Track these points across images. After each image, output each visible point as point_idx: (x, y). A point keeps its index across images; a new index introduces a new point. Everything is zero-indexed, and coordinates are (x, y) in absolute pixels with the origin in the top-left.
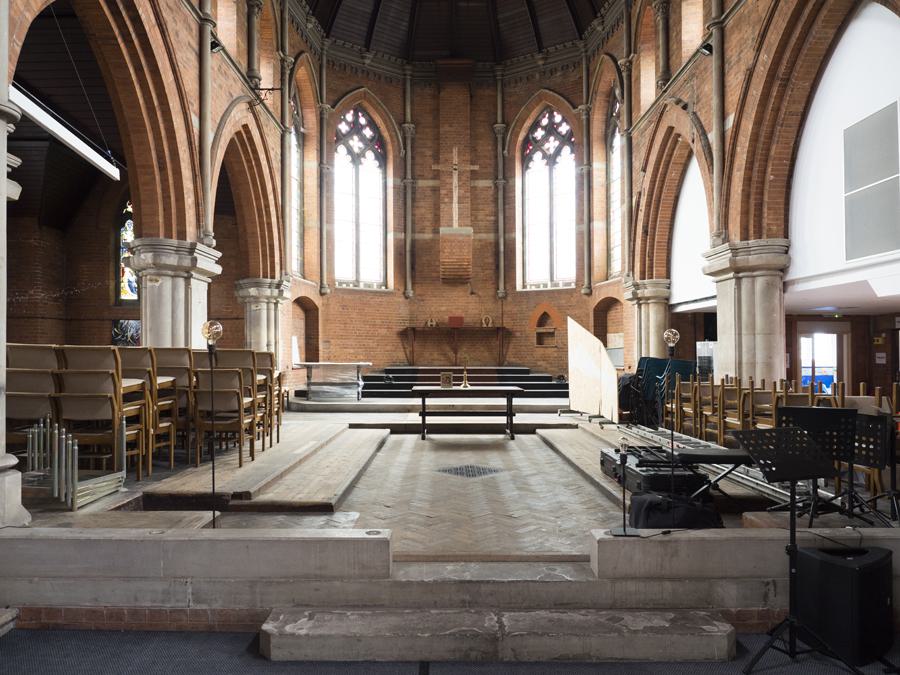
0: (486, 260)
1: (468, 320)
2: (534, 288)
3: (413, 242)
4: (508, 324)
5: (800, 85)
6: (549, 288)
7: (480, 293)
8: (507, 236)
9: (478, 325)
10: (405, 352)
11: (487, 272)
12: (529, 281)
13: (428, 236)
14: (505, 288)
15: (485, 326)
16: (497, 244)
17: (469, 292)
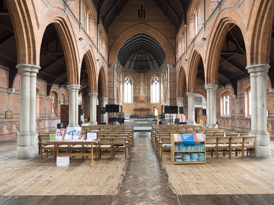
4: (150, 108)
12: (153, 102)
13: (138, 95)
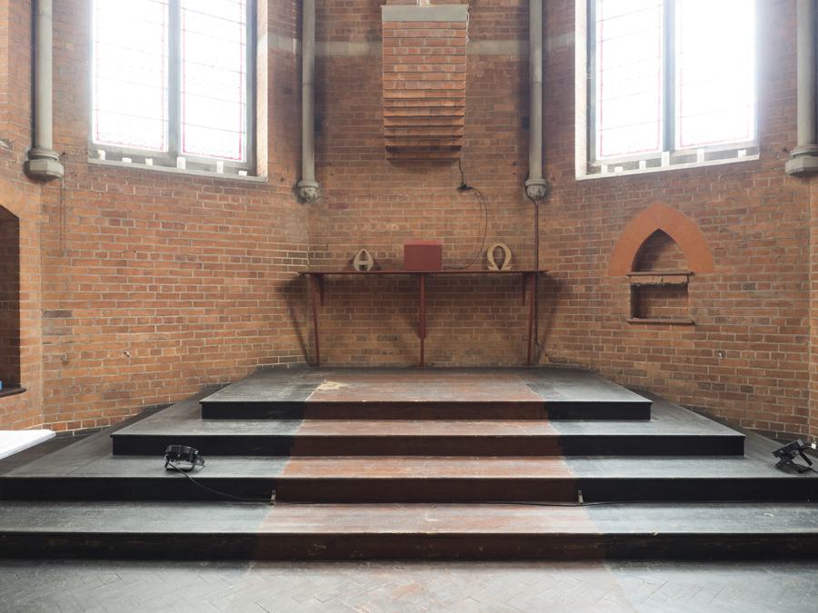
0: (498, 108)
1: (454, 255)
2: (619, 171)
3: (320, 64)
4: (550, 262)
5: (52, 543)
6: (666, 166)
7: (483, 188)
8: (550, 41)
9: (477, 267)
10: (298, 332)
11: (501, 135)
12: (600, 158)
13: (356, 47)
14: (544, 175)
15: (495, 268)
16: (525, 67)
17: (457, 185)
